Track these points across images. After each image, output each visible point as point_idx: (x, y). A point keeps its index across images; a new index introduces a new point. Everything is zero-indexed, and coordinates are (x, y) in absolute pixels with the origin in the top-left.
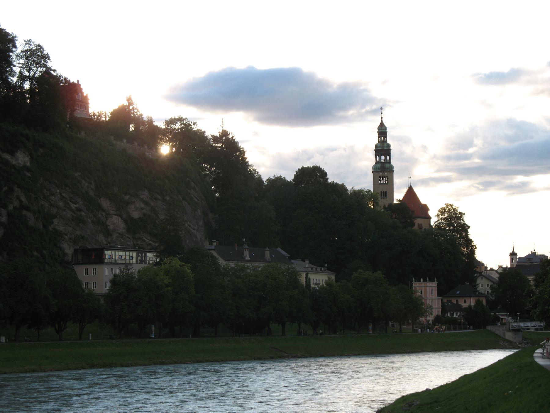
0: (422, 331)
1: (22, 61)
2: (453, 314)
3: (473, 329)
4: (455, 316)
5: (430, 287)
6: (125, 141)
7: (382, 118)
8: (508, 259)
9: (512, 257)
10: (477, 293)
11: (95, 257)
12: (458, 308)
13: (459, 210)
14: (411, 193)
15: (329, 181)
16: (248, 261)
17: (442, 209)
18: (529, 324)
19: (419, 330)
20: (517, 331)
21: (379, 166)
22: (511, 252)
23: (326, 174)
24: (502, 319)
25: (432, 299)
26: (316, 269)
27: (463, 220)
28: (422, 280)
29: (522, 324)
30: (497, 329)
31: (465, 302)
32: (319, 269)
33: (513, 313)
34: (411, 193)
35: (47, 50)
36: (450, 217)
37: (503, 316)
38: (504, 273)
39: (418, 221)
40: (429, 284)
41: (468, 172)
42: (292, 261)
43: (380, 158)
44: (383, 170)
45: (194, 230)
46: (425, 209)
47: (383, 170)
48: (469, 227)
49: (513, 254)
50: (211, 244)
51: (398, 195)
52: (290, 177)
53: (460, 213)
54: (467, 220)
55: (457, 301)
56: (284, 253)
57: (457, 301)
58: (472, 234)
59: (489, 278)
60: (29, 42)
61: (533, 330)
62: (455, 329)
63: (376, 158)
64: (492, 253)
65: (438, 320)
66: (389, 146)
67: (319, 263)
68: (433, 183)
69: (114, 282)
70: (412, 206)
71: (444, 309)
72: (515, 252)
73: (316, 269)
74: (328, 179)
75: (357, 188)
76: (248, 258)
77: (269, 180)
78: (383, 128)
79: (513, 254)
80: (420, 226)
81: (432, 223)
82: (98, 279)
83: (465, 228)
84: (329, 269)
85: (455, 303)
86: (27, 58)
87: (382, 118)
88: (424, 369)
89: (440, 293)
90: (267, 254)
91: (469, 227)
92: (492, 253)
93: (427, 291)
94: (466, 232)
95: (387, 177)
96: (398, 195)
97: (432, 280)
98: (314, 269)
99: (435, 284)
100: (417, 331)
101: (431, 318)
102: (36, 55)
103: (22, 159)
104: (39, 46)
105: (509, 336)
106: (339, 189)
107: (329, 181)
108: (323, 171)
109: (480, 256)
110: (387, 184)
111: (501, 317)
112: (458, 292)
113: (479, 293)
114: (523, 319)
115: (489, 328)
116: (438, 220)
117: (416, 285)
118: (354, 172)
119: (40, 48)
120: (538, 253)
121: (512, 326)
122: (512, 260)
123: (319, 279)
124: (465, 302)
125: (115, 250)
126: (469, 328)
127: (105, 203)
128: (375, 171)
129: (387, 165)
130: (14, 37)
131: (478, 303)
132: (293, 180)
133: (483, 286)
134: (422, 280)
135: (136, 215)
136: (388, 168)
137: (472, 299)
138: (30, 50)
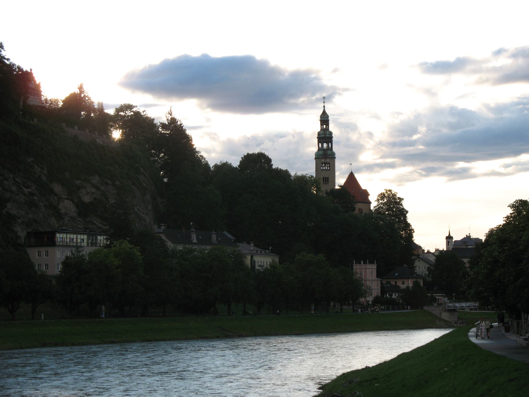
0: (362, 311)
2: (391, 295)
3: (411, 309)
4: (393, 296)
5: (369, 269)
7: (324, 107)
8: (444, 241)
9: (448, 240)
10: (415, 275)
11: (47, 240)
12: (396, 289)
13: (398, 195)
14: (351, 178)
15: (274, 167)
16: (195, 243)
17: (381, 194)
18: (464, 304)
19: (359, 310)
20: (452, 311)
22: (448, 235)
23: (270, 160)
24: (438, 299)
25: (372, 280)
26: (261, 252)
27: (401, 205)
28: (362, 262)
29: (457, 305)
30: (434, 310)
31: (403, 283)
32: (263, 252)
33: (449, 295)
34: (351, 178)
37: (439, 296)
38: (440, 255)
39: (359, 206)
40: (369, 266)
41: (410, 159)
42: (238, 244)
44: (326, 157)
45: (143, 213)
46: (365, 194)
47: (326, 157)
48: (407, 212)
49: (449, 238)
50: (159, 227)
51: (340, 181)
52: (235, 162)
53: (399, 198)
54: (406, 205)
55: (396, 282)
57: (396, 282)
58: (410, 219)
59: (426, 261)
61: (467, 310)
62: (394, 309)
63: (318, 145)
64: (429, 236)
65: (377, 301)
67: (263, 246)
68: (378, 169)
69: (66, 264)
70: (353, 191)
71: (383, 290)
72: (451, 235)
73: (261, 252)
74: (272, 165)
75: (299, 174)
76: (195, 241)
77: (216, 166)
78: (326, 116)
79: (449, 238)
80: (361, 211)
81: (372, 208)
82: (50, 261)
83: (403, 213)
84: (273, 251)
85: (394, 284)
87: (324, 107)
90: (214, 237)
91: (407, 212)
92: (429, 236)
93: (367, 273)
94: (405, 217)
95: (329, 163)
96: (340, 181)
97: (371, 262)
98: (259, 252)
99: (374, 266)
100: (357, 311)
101: (370, 299)
105: (445, 316)
106: (283, 175)
107: (274, 167)
108: (268, 157)
109: (417, 239)
110: (329, 170)
111: (438, 298)
112: (397, 274)
113: (417, 275)
114: (459, 300)
115: (426, 308)
116: (378, 205)
117: (357, 267)
118: (301, 163)
121: (448, 307)
122: (448, 243)
123: (264, 261)
124: (403, 283)
125: (67, 233)
126: (407, 309)
127: (57, 188)
131: (416, 284)
132: (239, 166)
133: (421, 268)
134: (362, 262)
135: (87, 199)
136: (329, 155)
137: (410, 281)
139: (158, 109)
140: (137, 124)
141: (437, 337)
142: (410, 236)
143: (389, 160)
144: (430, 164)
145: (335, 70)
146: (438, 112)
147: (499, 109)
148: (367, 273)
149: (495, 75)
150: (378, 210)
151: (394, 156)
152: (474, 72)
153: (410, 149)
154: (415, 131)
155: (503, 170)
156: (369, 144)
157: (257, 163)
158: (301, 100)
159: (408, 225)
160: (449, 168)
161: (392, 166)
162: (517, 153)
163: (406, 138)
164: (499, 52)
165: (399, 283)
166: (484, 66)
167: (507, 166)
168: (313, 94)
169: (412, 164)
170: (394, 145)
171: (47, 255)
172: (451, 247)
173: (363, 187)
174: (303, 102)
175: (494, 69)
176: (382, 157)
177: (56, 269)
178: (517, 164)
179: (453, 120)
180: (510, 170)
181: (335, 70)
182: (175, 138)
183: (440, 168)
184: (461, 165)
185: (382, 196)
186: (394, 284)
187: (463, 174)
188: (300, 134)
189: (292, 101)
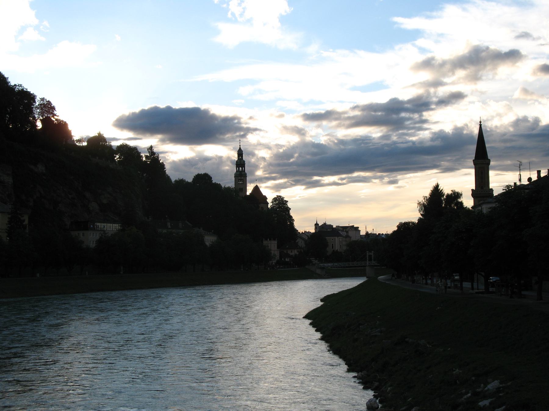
1: (38, 111)
2: (285, 259)
6: (97, 158)
11: (84, 226)
13: (285, 199)
14: (256, 189)
15: (213, 182)
20: (322, 268)
21: (238, 173)
23: (211, 178)
29: (326, 265)
34: (256, 189)
35: (54, 104)
36: (279, 203)
39: (261, 205)
41: (284, 174)
43: (239, 169)
46: (265, 198)
48: (290, 209)
49: (317, 225)
50: (148, 218)
52: (190, 179)
56: (189, 224)
60: (43, 99)
61: (329, 268)
64: (304, 224)
65: (278, 263)
66: (244, 162)
68: (265, 180)
69: (100, 242)
71: (281, 257)
75: (227, 186)
76: (169, 227)
77: (176, 181)
79: (317, 225)
80: (262, 208)
81: (269, 207)
82: (90, 239)
83: (288, 209)
86: (42, 109)
88: (258, 293)
89: (278, 247)
91: (290, 209)
92: (304, 224)
93: (272, 246)
97: (274, 240)
99: (276, 242)
101: (274, 261)
102: (48, 107)
103: (41, 168)
104: (49, 101)
105: (318, 271)
106: (218, 186)
107: (213, 182)
115: (307, 267)
117: (265, 243)
118: (226, 178)
119: (49, 103)
120: (328, 223)
122: (316, 228)
123: (209, 240)
125: (107, 223)
128: (236, 176)
129: (243, 173)
130: (35, 96)
135: (105, 201)
138: (44, 104)
139: (143, 143)
140: (129, 153)
141: (355, 286)
142: (292, 224)
143: (274, 175)
144: (297, 178)
145: (251, 118)
146: (305, 145)
147: (342, 142)
148: (272, 246)
149: (347, 122)
150: (272, 208)
151: (277, 173)
152: (336, 119)
153: (289, 169)
154: (292, 157)
155: (340, 182)
156: (262, 164)
157: (203, 180)
158: (227, 136)
159: (291, 217)
160: (308, 180)
161: (274, 179)
162: (351, 171)
163: (286, 161)
164: (354, 108)
165: (289, 252)
166: (343, 116)
167: (342, 179)
168: (235, 133)
169: (287, 178)
170: (279, 165)
171: (83, 235)
172: (318, 230)
173: (264, 194)
174: (228, 137)
175: (349, 118)
176: (270, 173)
177: (93, 245)
178: (349, 178)
179: (315, 150)
180: (344, 181)
181: (251, 118)
182: (154, 162)
183: (303, 180)
184: (316, 178)
185: (275, 199)
186: (286, 252)
187: (317, 184)
188: (221, 157)
189: (222, 137)
